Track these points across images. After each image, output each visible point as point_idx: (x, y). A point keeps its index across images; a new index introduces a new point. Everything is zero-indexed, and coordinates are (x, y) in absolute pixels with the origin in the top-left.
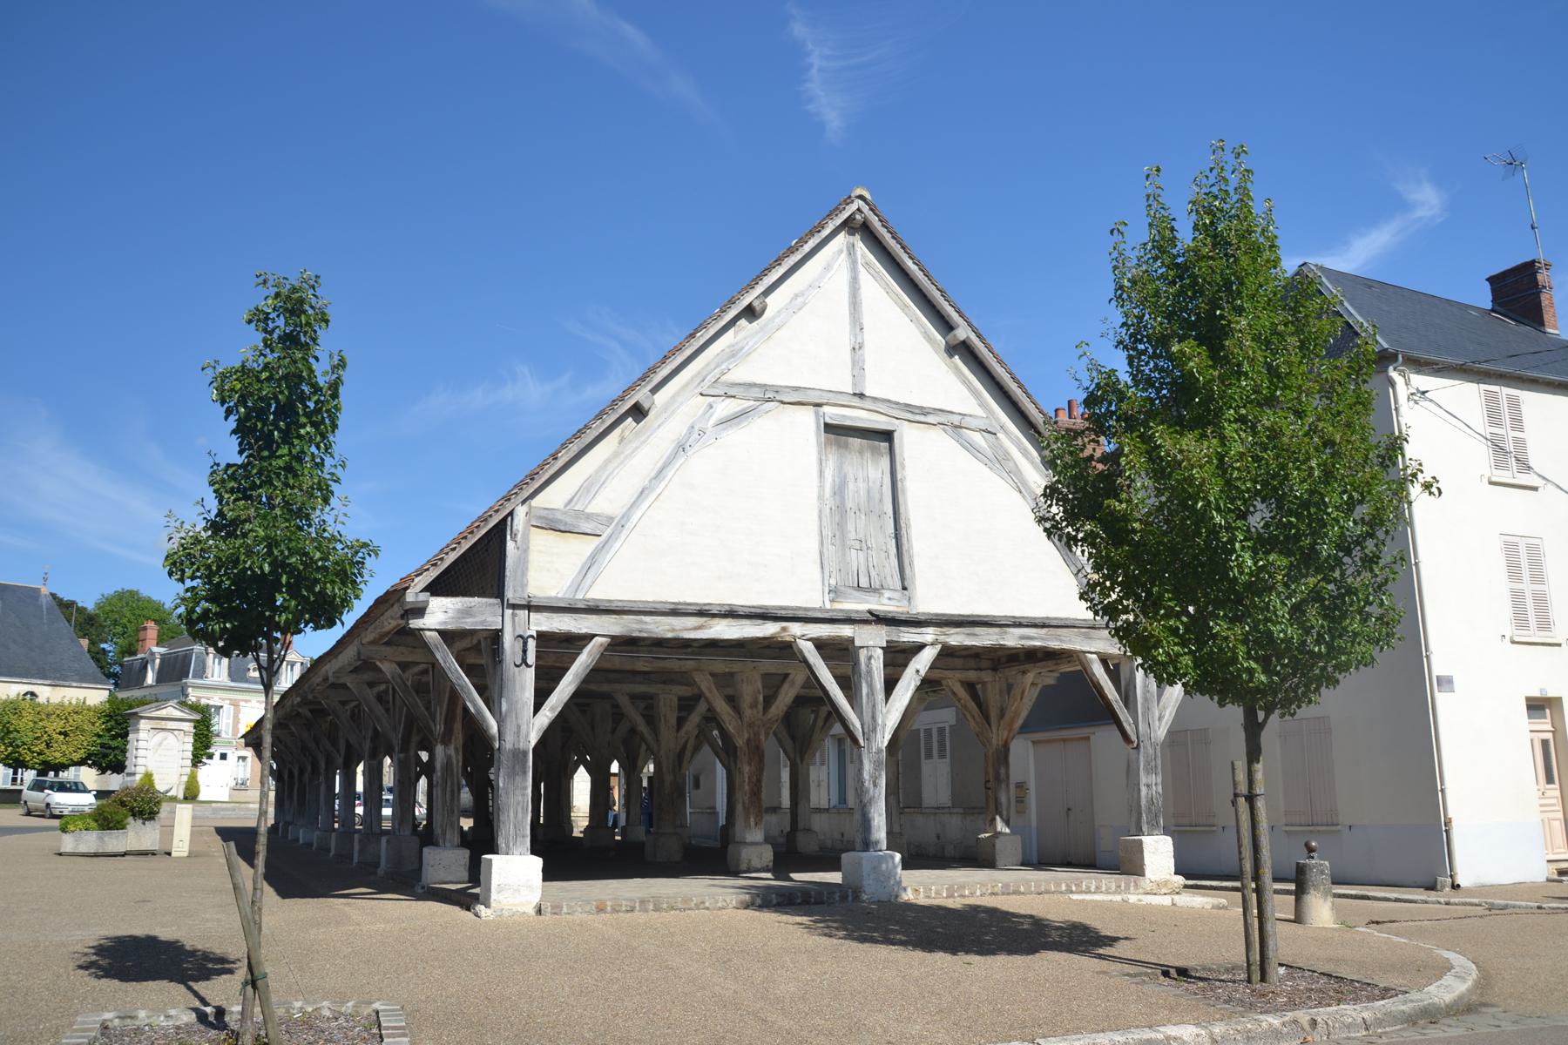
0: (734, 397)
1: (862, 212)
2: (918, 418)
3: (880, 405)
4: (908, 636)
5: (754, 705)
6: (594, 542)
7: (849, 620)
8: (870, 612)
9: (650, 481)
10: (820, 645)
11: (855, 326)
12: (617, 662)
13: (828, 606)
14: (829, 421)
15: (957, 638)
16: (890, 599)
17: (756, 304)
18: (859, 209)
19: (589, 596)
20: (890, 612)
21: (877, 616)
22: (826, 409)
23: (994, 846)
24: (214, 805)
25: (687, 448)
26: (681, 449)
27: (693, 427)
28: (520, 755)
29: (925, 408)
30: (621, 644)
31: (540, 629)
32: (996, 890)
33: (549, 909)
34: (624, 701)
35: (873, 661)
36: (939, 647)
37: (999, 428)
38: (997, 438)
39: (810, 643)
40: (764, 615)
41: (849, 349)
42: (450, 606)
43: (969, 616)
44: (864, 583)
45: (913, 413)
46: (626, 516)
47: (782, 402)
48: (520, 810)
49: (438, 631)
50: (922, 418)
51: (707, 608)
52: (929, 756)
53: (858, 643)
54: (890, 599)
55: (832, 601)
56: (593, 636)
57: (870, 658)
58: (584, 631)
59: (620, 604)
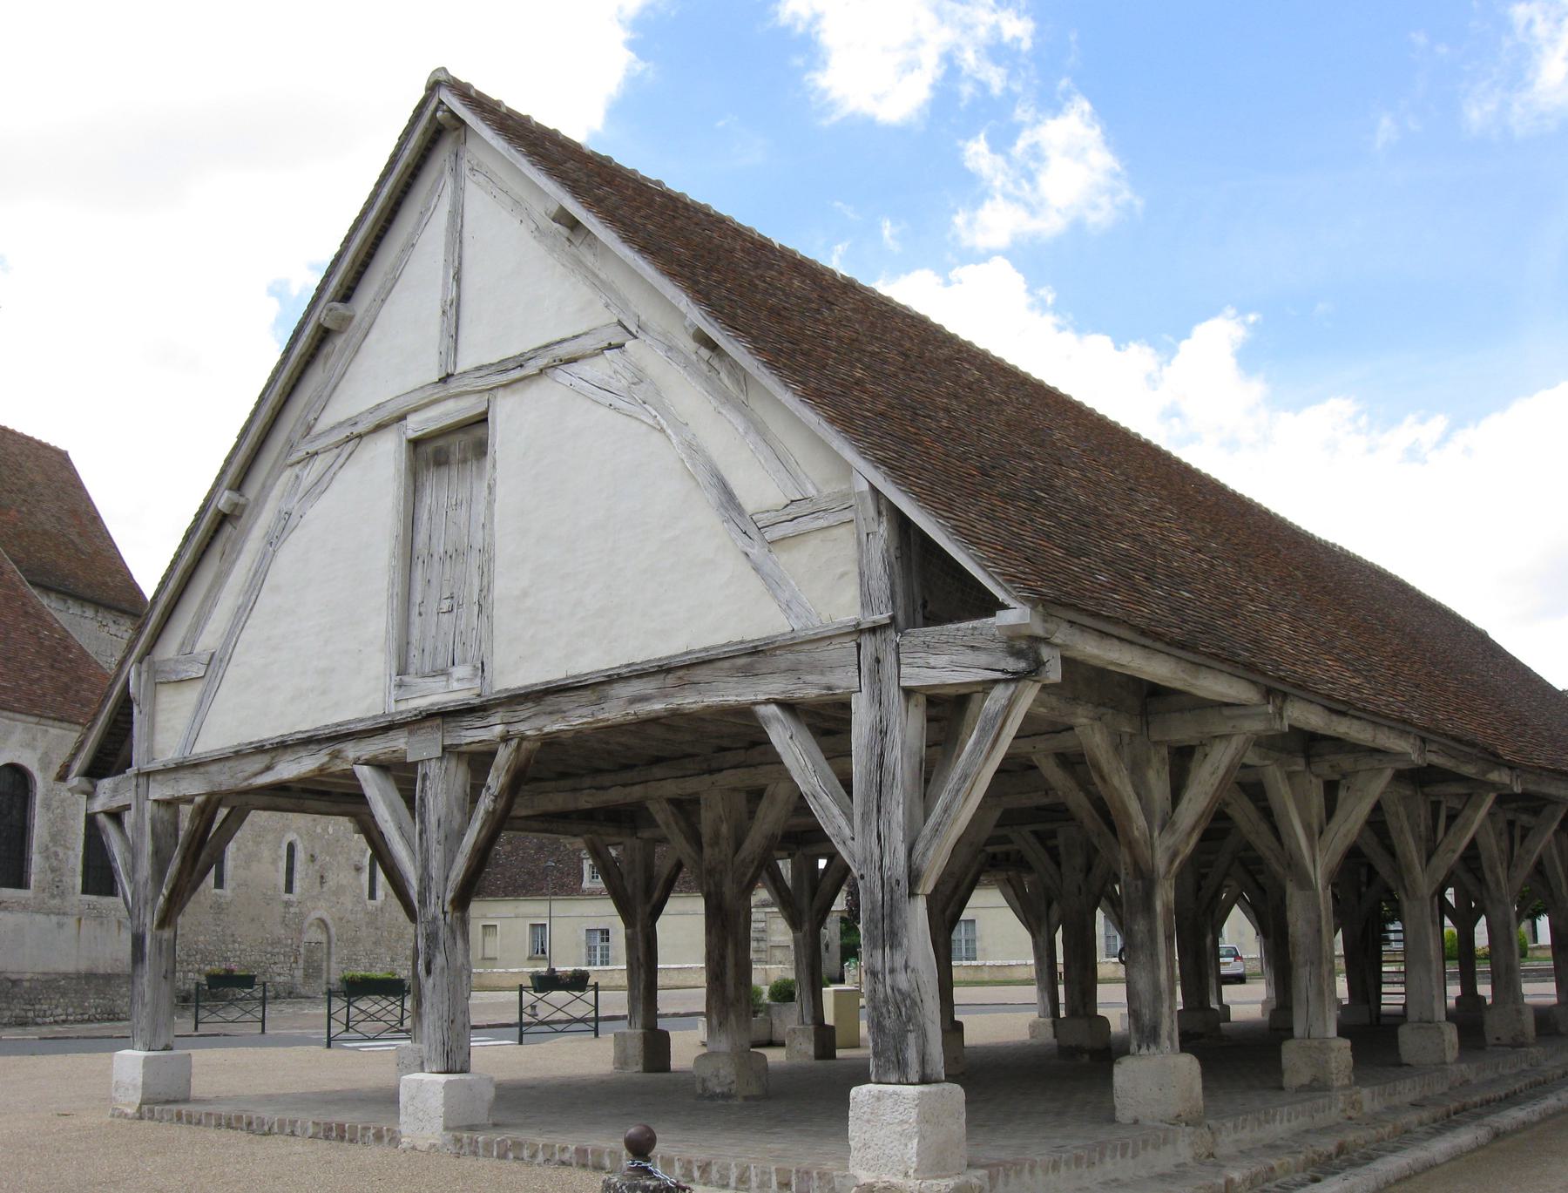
0: (317, 453)
4: (472, 735)
20: (438, 704)
32: (566, 1156)
40: (310, 741)
47: (360, 436)
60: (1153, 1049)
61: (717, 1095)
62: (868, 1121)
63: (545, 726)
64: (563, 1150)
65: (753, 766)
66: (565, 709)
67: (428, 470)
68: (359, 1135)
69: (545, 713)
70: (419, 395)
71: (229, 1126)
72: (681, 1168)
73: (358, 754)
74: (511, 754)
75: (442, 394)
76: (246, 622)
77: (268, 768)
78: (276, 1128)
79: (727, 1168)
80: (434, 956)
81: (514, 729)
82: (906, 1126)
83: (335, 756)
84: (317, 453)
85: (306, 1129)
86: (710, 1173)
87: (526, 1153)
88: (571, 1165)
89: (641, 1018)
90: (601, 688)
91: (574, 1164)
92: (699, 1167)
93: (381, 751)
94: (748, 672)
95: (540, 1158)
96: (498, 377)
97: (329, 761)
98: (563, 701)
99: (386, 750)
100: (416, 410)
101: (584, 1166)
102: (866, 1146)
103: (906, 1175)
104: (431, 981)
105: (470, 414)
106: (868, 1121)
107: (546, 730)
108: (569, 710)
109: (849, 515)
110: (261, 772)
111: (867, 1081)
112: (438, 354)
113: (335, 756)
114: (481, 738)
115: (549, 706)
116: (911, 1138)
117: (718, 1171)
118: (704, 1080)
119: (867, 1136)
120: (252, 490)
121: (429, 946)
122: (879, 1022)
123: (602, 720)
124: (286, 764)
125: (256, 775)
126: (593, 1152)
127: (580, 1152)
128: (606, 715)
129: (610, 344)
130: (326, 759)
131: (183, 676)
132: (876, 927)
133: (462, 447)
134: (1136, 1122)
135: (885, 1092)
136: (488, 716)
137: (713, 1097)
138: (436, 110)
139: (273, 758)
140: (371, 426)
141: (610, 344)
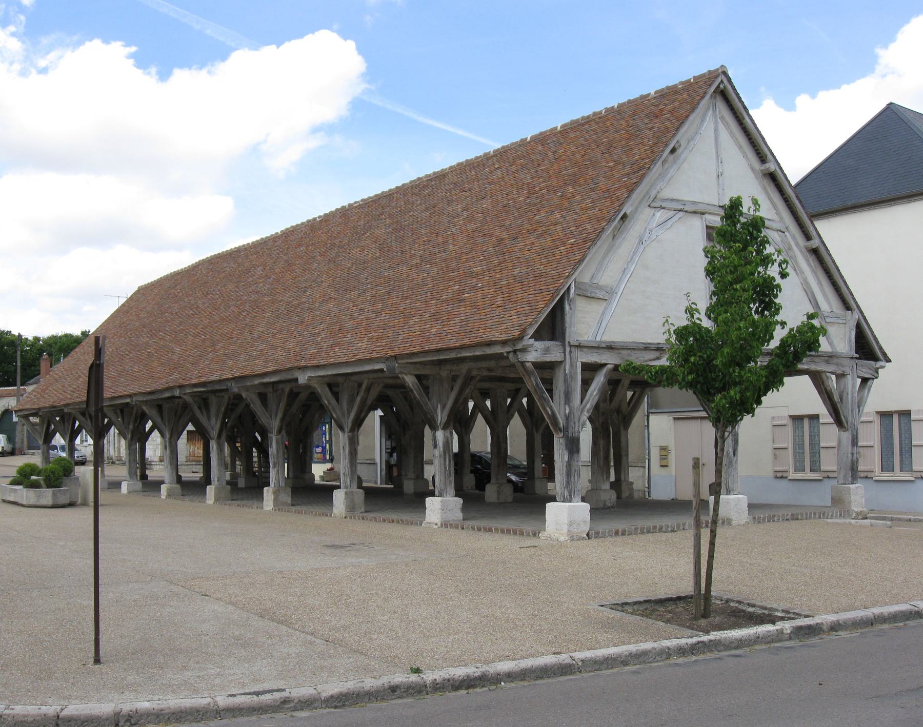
0: (664, 208)
22: (707, 216)
24: (647, 430)
32: (788, 517)
47: (686, 212)
71: (649, 532)
85: (679, 527)
87: (776, 519)
89: (356, 483)
94: (827, 362)
100: (710, 213)
101: (794, 519)
109: (844, 322)
110: (654, 360)
118: (605, 501)
125: (651, 360)
127: (793, 515)
131: (593, 295)
137: (609, 508)
138: (719, 84)
139: (661, 354)
140: (692, 210)
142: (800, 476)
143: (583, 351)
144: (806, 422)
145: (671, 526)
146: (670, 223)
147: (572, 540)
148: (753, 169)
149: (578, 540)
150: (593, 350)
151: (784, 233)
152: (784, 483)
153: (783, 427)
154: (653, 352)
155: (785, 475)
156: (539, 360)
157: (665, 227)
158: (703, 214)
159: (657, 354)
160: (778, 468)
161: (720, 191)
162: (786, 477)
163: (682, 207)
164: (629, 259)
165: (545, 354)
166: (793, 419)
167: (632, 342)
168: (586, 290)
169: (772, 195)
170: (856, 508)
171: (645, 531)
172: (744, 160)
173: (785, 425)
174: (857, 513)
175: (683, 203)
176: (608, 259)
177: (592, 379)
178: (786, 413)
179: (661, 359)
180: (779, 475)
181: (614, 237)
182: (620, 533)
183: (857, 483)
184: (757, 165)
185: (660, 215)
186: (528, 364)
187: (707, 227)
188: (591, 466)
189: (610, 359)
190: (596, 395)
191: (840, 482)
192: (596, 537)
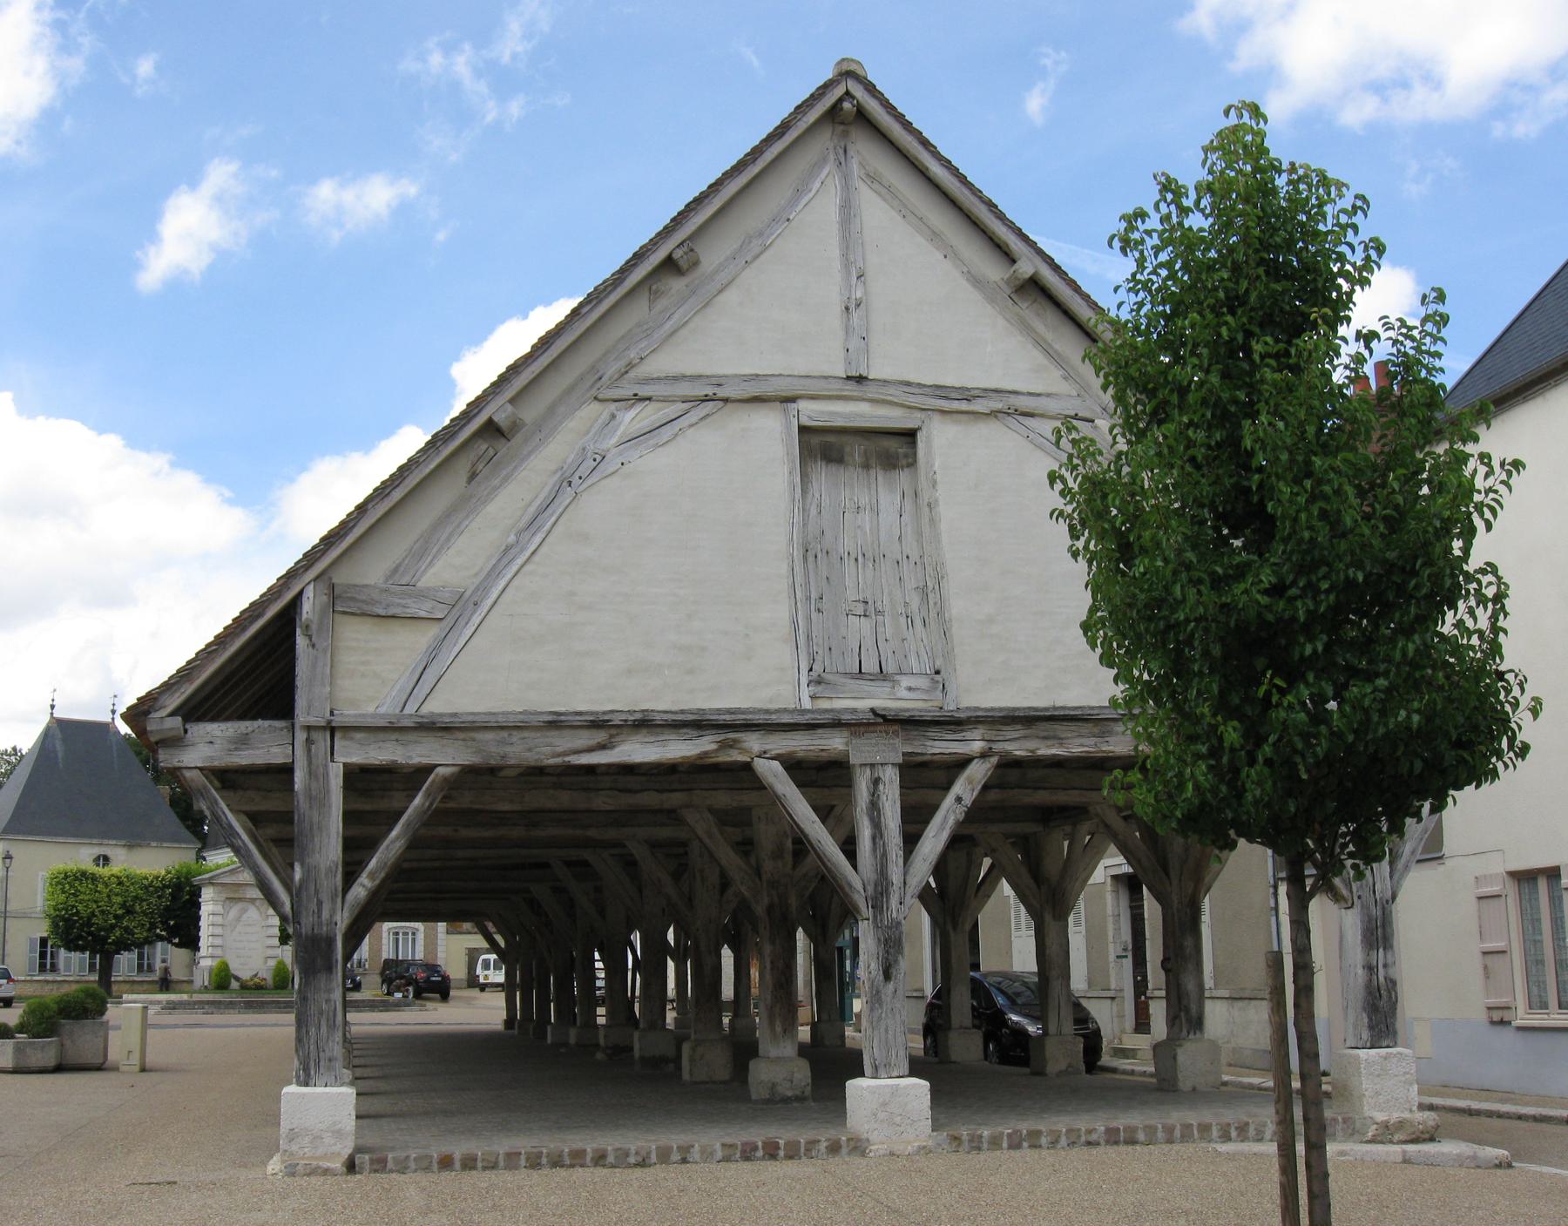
0: (649, 399)
1: (853, 97)
2: (956, 405)
3: (891, 391)
4: (941, 746)
5: (778, 854)
6: (432, 632)
7: (836, 724)
8: (873, 710)
9: (519, 534)
10: (795, 767)
11: (848, 273)
12: (465, 800)
13: (807, 704)
14: (806, 422)
15: (1019, 746)
16: (910, 689)
17: (677, 255)
18: (847, 93)
19: (425, 710)
20: (908, 710)
21: (883, 717)
22: (803, 405)
23: (1175, 1058)
24: (1274, 919)
25: (575, 480)
26: (565, 484)
27: (584, 449)
28: (323, 945)
29: (968, 389)
30: (472, 775)
31: (349, 760)
32: (1094, 1137)
33: (367, 1166)
34: (639, 851)
35: (881, 787)
36: (994, 760)
37: (1099, 410)
38: (1096, 427)
39: (776, 763)
40: (698, 724)
41: (838, 309)
42: (219, 733)
43: (1046, 709)
44: (870, 666)
45: (946, 398)
46: (483, 588)
47: (726, 400)
48: (323, 1022)
49: (201, 769)
50: (964, 406)
51: (606, 718)
52: (1018, 929)
53: (854, 760)
54: (910, 689)
55: (813, 697)
56: (433, 767)
57: (876, 782)
58: (416, 760)
59: (470, 718)
60: (1198, 1035)
61: (789, 1098)
62: (1378, 1076)
63: (1039, 749)
64: (1089, 1132)
65: (828, 787)
66: (1063, 736)
67: (816, 461)
68: (802, 1150)
69: (1038, 737)
70: (823, 383)
72: (1218, 1131)
73: (767, 747)
74: (990, 769)
75: (855, 394)
76: (522, 566)
77: (602, 747)
78: (654, 1158)
79: (1265, 1125)
80: (896, 961)
81: (998, 747)
82: (1408, 1076)
83: (725, 745)
84: (649, 399)
86: (1248, 1131)
88: (1098, 1144)
90: (1106, 723)
91: (1102, 1142)
92: (1237, 1128)
93: (803, 748)
95: (1063, 1141)
96: (933, 400)
97: (716, 751)
98: (1060, 729)
99: (812, 748)
101: (1116, 1143)
102: (1378, 1093)
103: (1411, 1111)
104: (891, 986)
105: (891, 426)
106: (1378, 1076)
107: (1040, 752)
108: (1068, 738)
110: (590, 750)
111: (862, 1075)
112: (843, 353)
113: (725, 745)
114: (954, 751)
115: (1043, 731)
116: (1411, 1084)
117: (1255, 1129)
118: (774, 1085)
119: (1378, 1087)
120: (530, 413)
121: (887, 952)
122: (1374, 1004)
123: (1104, 752)
124: (638, 746)
126: (1125, 1129)
127: (1109, 1131)
128: (1111, 748)
129: (1076, 415)
130: (714, 746)
132: (1372, 934)
133: (862, 451)
134: (1194, 1089)
135: (1391, 1054)
136: (962, 731)
137: (786, 1100)
139: (612, 736)
141: (1076, 415)
142: (1537, 1020)
143: (352, 739)
144: (1542, 884)
145: (637, 1153)
146: (668, 432)
147: (293, 1174)
148: (977, 281)
149: (308, 1175)
150: (381, 736)
151: (1093, 421)
152: (1507, 1035)
153: (1496, 900)
154: (585, 733)
155: (1507, 1016)
156: (216, 763)
157: (652, 442)
158: (793, 400)
159: (600, 736)
160: (1493, 1001)
161: (855, 343)
162: (1509, 1023)
163: (709, 391)
164: (522, 524)
165: (236, 749)
166: (1519, 881)
167: (524, 713)
168: (374, 602)
169: (1049, 336)
170: (1377, 1113)
171: (544, 1160)
172: (947, 265)
173: (1499, 896)
174: (1386, 1126)
175: (714, 381)
176: (448, 530)
177: (933, 809)
178: (1499, 866)
179: (613, 747)
180: (1496, 1016)
181: (473, 476)
182: (457, 1165)
183: (1395, 1045)
184: (994, 271)
185: (632, 419)
186: (188, 774)
187: (803, 430)
188: (1168, 998)
189: (446, 757)
190: (397, 838)
191: (1348, 1045)
192: (376, 1171)
